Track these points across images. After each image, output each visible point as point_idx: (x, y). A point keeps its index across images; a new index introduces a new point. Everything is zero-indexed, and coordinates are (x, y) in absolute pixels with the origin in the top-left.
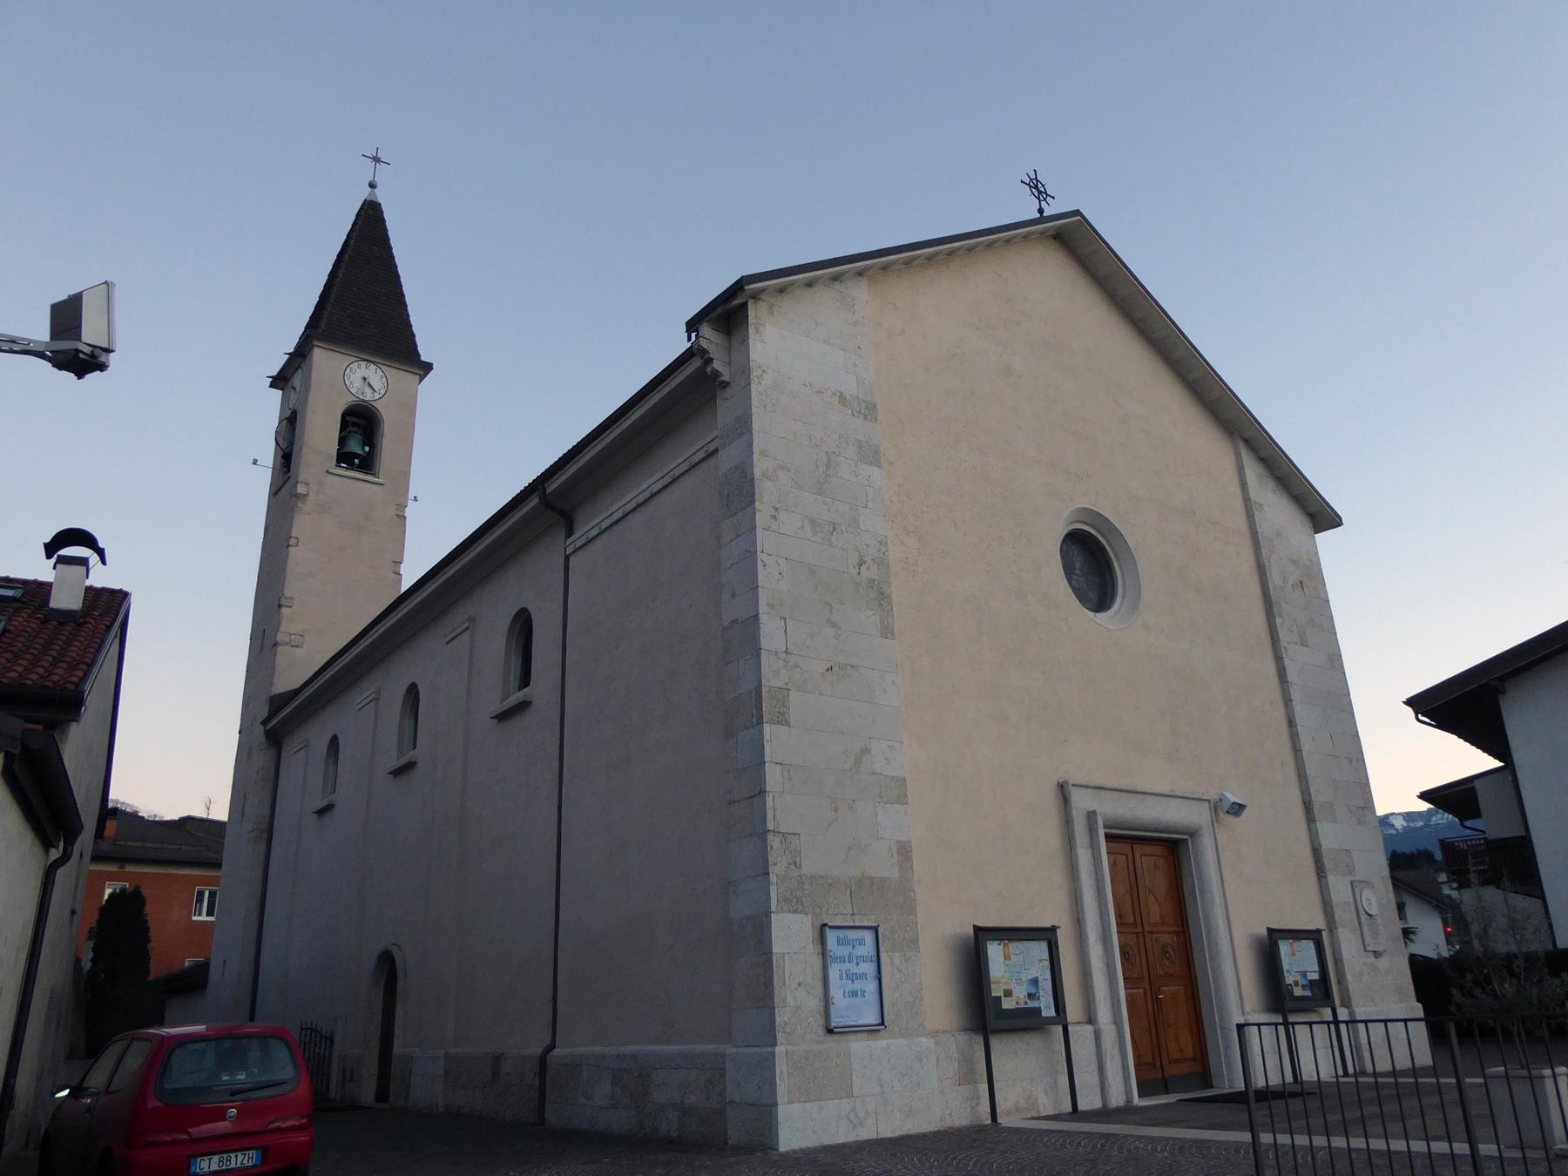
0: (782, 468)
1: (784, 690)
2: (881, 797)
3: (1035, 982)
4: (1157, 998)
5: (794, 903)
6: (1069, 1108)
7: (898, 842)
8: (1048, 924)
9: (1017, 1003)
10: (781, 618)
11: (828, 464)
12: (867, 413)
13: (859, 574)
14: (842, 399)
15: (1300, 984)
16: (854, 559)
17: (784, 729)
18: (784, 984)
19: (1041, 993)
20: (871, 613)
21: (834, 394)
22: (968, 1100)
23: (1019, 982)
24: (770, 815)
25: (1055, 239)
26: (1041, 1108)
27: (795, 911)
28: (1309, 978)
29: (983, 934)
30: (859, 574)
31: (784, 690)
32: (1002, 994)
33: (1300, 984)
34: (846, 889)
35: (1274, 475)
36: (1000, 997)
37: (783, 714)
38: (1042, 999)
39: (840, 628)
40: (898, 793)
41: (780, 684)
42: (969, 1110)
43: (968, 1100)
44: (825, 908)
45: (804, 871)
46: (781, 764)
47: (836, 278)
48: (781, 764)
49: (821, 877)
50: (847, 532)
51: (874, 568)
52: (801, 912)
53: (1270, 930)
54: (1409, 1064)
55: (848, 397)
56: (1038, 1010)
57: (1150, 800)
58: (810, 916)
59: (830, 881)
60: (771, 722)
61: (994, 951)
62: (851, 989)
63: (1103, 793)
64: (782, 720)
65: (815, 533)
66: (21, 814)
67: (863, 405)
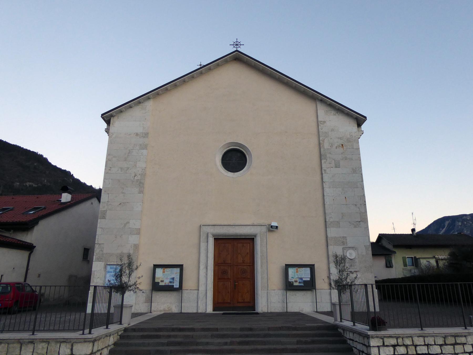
0: (114, 157)
1: (106, 211)
2: (131, 234)
3: (173, 279)
4: (235, 284)
5: (99, 260)
6: (316, 311)
7: (134, 244)
8: (313, 264)
9: (165, 284)
10: (108, 194)
11: (129, 153)
12: (145, 136)
13: (134, 179)
14: (137, 134)
15: (298, 282)
16: (133, 175)
17: (104, 220)
18: (94, 277)
19: (175, 282)
20: (136, 188)
21: (134, 134)
22: (147, 306)
23: (167, 279)
24: (96, 240)
25: (235, 60)
26: (173, 311)
27: (100, 261)
28: (303, 280)
29: (288, 266)
30: (134, 179)
31: (106, 211)
32: (160, 281)
33: (298, 282)
34: (116, 256)
35: (336, 109)
36: (159, 282)
37: (104, 216)
38: (175, 283)
39: (125, 193)
40: (138, 232)
41: (104, 209)
42: (147, 309)
43: (147, 306)
44: (109, 260)
45: (104, 252)
46: (102, 228)
47: (140, 103)
48: (102, 228)
49: (109, 253)
50: (132, 169)
51: (139, 176)
52: (101, 261)
53: (286, 265)
54: (364, 309)
55: (139, 134)
56: (173, 286)
57: (237, 227)
58: (104, 262)
59: (111, 254)
60: (100, 219)
61: (291, 271)
62: (112, 279)
63: (216, 227)
64: (104, 218)
65: (122, 171)
66: (12, 249)
67: (144, 134)
